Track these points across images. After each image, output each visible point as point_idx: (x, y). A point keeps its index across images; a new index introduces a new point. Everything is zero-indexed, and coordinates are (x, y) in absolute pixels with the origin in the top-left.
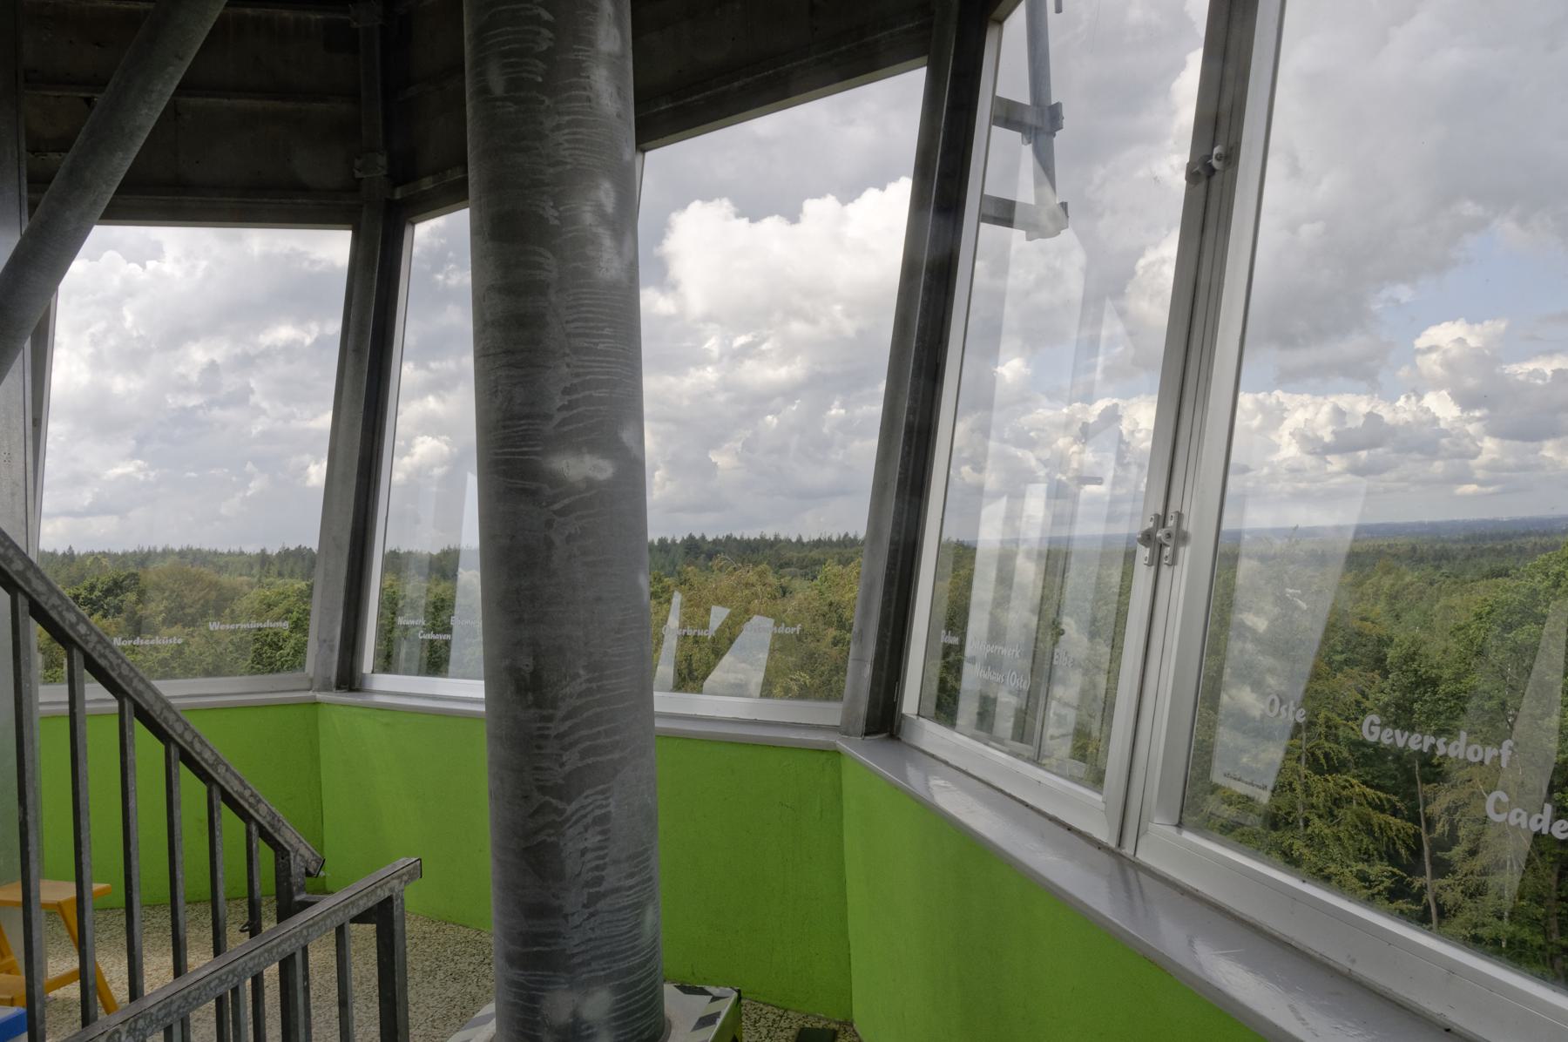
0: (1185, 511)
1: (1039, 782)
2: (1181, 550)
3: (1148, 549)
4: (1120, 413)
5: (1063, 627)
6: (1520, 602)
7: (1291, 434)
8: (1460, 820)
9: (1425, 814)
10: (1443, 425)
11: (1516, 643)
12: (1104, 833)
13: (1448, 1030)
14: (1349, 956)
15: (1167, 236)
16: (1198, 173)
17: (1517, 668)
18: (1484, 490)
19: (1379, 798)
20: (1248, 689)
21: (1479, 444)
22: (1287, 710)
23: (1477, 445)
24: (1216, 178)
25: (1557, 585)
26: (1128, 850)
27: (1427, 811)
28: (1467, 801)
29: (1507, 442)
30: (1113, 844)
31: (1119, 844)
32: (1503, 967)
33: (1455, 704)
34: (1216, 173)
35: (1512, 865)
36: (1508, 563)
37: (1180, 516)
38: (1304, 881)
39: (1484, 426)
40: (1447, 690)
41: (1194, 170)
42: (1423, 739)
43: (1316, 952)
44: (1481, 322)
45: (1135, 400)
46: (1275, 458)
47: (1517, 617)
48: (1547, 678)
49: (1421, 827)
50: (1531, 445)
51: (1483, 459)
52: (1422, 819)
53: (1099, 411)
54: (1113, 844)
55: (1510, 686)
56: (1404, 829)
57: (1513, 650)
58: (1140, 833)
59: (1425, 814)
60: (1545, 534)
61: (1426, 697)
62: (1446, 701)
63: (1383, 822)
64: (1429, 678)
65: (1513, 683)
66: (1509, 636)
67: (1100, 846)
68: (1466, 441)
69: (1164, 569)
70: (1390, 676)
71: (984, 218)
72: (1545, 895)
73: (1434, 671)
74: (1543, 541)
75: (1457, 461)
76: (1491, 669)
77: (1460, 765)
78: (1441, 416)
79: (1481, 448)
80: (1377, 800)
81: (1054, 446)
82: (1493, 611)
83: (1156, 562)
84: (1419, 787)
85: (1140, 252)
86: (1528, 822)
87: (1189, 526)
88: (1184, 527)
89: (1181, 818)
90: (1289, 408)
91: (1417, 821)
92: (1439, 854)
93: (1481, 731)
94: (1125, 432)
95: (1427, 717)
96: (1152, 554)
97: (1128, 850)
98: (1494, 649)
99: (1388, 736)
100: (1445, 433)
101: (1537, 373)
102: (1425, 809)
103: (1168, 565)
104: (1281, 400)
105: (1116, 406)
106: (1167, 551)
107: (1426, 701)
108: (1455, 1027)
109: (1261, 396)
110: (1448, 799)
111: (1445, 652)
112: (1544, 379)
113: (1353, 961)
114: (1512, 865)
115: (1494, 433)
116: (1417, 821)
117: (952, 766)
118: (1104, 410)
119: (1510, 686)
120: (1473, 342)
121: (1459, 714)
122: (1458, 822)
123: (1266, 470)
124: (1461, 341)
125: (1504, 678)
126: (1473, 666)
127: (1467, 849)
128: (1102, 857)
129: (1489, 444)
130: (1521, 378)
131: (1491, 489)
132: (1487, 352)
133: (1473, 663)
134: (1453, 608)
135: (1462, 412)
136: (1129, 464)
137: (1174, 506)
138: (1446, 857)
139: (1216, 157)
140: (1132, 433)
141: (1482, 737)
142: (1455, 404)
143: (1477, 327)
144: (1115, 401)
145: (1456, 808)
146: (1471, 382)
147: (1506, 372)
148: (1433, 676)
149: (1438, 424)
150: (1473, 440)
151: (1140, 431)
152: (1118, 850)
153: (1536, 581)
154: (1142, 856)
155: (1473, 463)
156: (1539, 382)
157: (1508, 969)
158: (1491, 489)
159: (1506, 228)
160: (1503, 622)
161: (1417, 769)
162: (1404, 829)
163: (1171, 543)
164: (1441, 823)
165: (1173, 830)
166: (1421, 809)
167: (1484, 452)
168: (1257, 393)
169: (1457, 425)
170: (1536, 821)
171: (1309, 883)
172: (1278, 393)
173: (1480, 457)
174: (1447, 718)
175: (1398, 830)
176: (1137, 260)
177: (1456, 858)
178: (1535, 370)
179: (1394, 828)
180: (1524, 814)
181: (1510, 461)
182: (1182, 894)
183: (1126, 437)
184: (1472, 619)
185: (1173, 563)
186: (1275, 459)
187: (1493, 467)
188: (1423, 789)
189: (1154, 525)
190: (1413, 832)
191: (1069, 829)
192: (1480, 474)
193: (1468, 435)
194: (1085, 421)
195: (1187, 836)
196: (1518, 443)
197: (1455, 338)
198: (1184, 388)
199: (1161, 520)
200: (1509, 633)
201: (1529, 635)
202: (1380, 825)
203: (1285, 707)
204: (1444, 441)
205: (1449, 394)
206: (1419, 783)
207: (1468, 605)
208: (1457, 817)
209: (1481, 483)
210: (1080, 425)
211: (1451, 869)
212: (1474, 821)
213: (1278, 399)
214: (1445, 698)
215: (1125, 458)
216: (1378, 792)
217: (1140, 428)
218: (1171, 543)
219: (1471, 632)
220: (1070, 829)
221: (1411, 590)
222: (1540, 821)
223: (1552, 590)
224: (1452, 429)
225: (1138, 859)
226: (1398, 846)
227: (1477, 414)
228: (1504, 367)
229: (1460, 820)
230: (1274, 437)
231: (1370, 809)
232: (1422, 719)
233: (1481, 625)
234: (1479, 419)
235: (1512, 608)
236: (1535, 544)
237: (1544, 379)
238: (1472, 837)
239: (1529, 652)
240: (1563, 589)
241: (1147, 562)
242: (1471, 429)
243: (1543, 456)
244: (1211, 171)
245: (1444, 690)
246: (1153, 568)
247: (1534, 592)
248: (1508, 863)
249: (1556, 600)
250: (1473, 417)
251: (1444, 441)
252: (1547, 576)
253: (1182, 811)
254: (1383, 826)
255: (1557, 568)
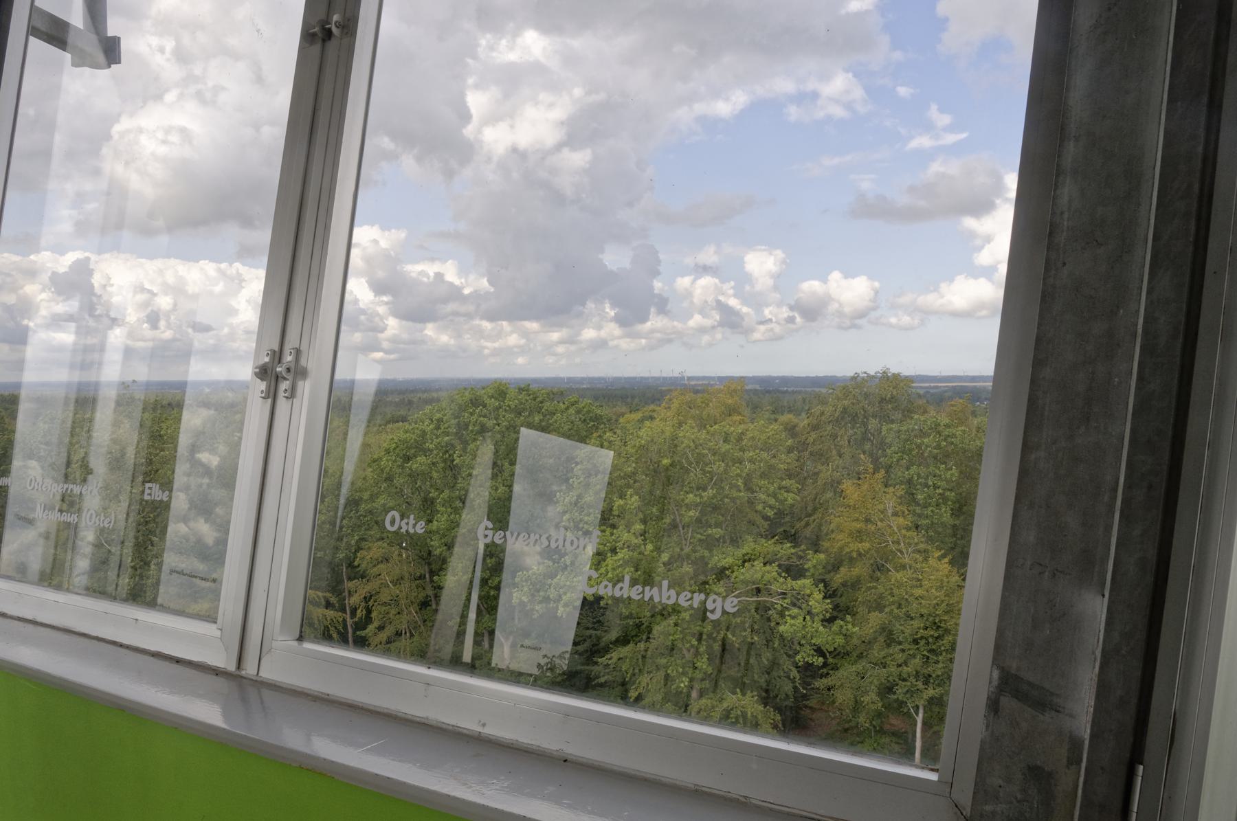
0: (304, 348)
1: (137, 620)
2: (300, 384)
3: (265, 383)
4: (91, 267)
5: (91, 465)
6: (415, 440)
7: (247, 301)
8: (373, 605)
9: (349, 604)
10: (361, 305)
11: (412, 470)
12: (222, 659)
13: (565, 761)
14: (480, 721)
15: (142, 107)
16: (314, 35)
17: (411, 489)
18: (388, 356)
19: (318, 597)
20: (202, 521)
21: (385, 321)
22: (407, 524)
23: (384, 323)
24: (332, 45)
25: (438, 428)
26: (250, 669)
27: (351, 602)
28: (378, 590)
29: (404, 322)
30: (232, 667)
31: (239, 666)
32: (598, 703)
33: (371, 518)
34: (333, 39)
35: (406, 633)
36: (403, 412)
37: (298, 352)
38: (429, 668)
39: (389, 308)
40: (366, 508)
41: (311, 31)
42: (505, 535)
43: (449, 725)
44: (389, 230)
45: (107, 256)
46: (235, 321)
47: (413, 451)
48: (431, 495)
49: (346, 613)
50: (419, 326)
51: (389, 333)
52: (347, 608)
53: (70, 263)
54: (232, 667)
55: (407, 502)
56: (335, 618)
57: (410, 475)
58: (263, 654)
59: (349, 604)
60: (425, 391)
61: (352, 514)
62: (365, 516)
63: (321, 616)
64: (354, 499)
65: (409, 500)
66: (408, 465)
67: (217, 672)
68: (377, 319)
69: (282, 404)
70: (326, 500)
71: (33, 31)
72: (742, 639)
73: (357, 494)
74: (425, 397)
75: (370, 334)
76: (394, 490)
77: (373, 564)
78: (360, 299)
79: (387, 325)
80: (316, 598)
81: (21, 292)
82: (397, 447)
83: (272, 395)
84: (346, 584)
85: (116, 119)
86: (613, 591)
87: (309, 362)
88: (303, 362)
89: (301, 632)
90: (246, 279)
91: (343, 610)
92: (358, 633)
93: (388, 537)
94: (96, 285)
95: (352, 530)
96: (268, 387)
97: (250, 669)
98: (398, 475)
99: (500, 537)
100: (363, 312)
101: (422, 273)
102: (349, 600)
103: (287, 397)
104: (240, 271)
105: (88, 259)
106: (284, 385)
107: (351, 517)
108: (569, 757)
109: (223, 266)
110: (365, 590)
111: (364, 479)
112: (428, 278)
113: (484, 725)
114: (406, 633)
115: (396, 314)
116: (343, 610)
117: (12, 618)
118: (75, 261)
119: (407, 502)
120: (384, 244)
121: (373, 526)
122: (372, 607)
123: (226, 330)
124: (376, 242)
125: (403, 496)
126: (382, 489)
127: (377, 626)
128: (220, 682)
129: (392, 322)
130: (414, 275)
131: (392, 357)
132: (392, 253)
133: (383, 486)
134: (369, 445)
135: (375, 296)
136: (100, 316)
137: (292, 341)
138: (363, 635)
139: (335, 24)
140: (104, 287)
141: (388, 542)
142: (370, 290)
143: (387, 233)
144: (87, 254)
145: (370, 598)
146: (381, 274)
147: (405, 269)
148: (357, 498)
149: (359, 305)
150: (382, 319)
151: (112, 285)
152: (238, 673)
153: (425, 424)
154: (267, 674)
155: (381, 336)
156: (425, 280)
157: (600, 703)
158: (392, 357)
159: (408, 162)
160: (404, 455)
161: (344, 570)
162: (335, 618)
163: (290, 377)
164: (360, 609)
165: (295, 643)
166: (347, 602)
167: (388, 328)
168: (221, 263)
169: (371, 306)
170: (619, 589)
171: (434, 669)
172: (237, 265)
173: (386, 332)
174: (366, 530)
175: (331, 619)
176: (112, 125)
177: (370, 635)
178: (422, 271)
179: (328, 619)
180: (610, 585)
181: (405, 336)
182: (315, 701)
183: (97, 290)
184: (383, 453)
185: (292, 394)
186: (234, 322)
187: (394, 340)
188: (349, 585)
189: (270, 359)
190: (342, 619)
191: (177, 662)
192: (385, 345)
193: (378, 315)
194: (55, 270)
195: (308, 645)
196: (410, 324)
197: (372, 239)
198: (300, 233)
199: (278, 356)
200: (407, 463)
201: (420, 464)
202: (318, 617)
203: (405, 521)
204: (362, 317)
205: (367, 282)
206: (345, 581)
207: (379, 443)
208: (371, 603)
209: (386, 352)
210: (49, 274)
211: (367, 643)
212: (382, 604)
213: (238, 270)
214: (364, 514)
215: (96, 309)
216: (317, 592)
217: (111, 282)
218: (290, 377)
219: (383, 463)
220: (178, 661)
221: (337, 432)
222: (621, 588)
223: (435, 431)
224: (368, 309)
225: (261, 677)
226: (331, 632)
227: (385, 299)
228: (404, 266)
229: (373, 605)
230: (234, 303)
231: (311, 606)
232: (348, 532)
233: (389, 458)
234: (387, 303)
235: (409, 444)
236: (420, 398)
237: (428, 278)
238: (381, 616)
239: (420, 476)
240: (442, 431)
241: (263, 395)
242: (381, 310)
243: (426, 335)
244: (328, 34)
245: (364, 508)
246: (269, 401)
247: (424, 433)
248: (403, 632)
249: (437, 438)
250: (382, 301)
251: (362, 317)
252: (432, 420)
253: (302, 626)
254: (320, 618)
255: (438, 416)
